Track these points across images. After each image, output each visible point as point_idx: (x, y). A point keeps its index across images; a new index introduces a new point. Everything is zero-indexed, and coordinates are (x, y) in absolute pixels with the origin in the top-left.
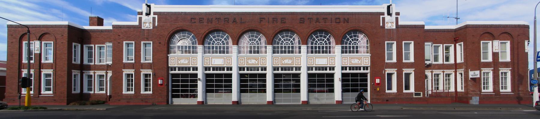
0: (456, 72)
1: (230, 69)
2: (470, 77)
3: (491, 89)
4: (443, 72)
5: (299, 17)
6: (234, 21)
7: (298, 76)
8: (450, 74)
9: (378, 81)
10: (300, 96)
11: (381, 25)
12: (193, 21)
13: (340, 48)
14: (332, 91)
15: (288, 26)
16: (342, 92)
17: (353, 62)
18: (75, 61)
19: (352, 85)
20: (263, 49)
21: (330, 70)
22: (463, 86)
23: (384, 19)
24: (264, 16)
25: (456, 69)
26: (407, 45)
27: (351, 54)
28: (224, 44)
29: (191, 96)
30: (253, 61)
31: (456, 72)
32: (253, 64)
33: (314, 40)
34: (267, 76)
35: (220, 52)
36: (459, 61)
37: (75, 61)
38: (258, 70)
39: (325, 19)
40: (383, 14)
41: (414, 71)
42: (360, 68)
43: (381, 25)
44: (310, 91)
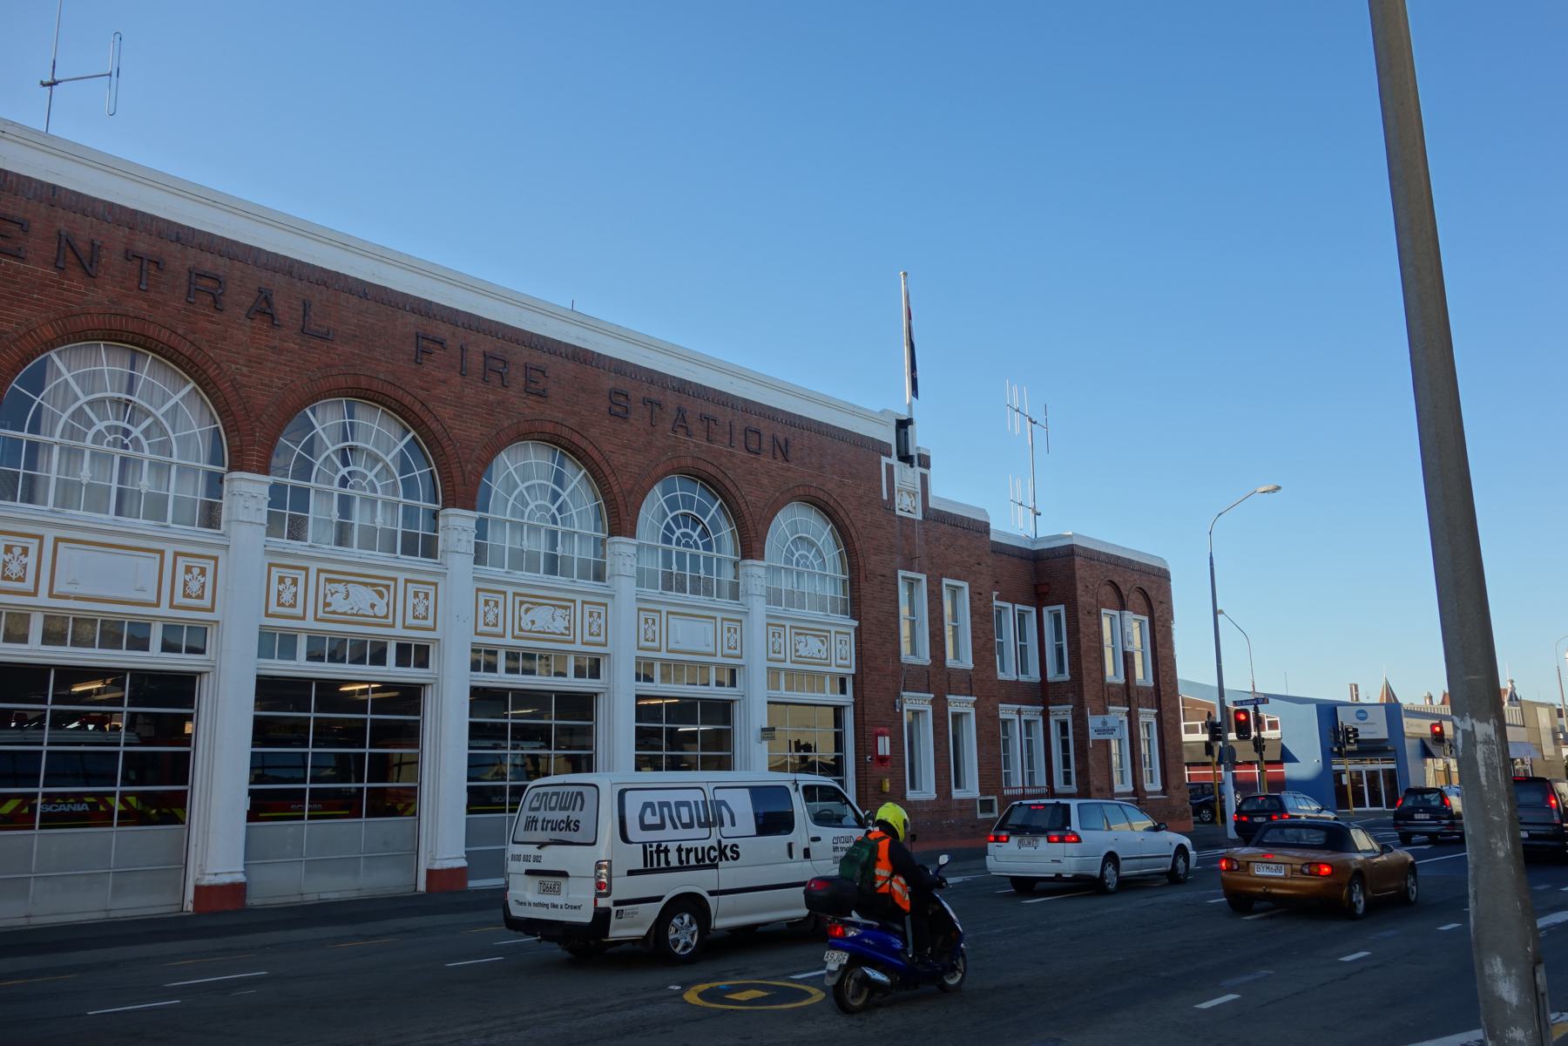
0: (1046, 715)
1: (193, 638)
5: (609, 382)
7: (180, 689)
8: (961, 714)
9: (884, 746)
11: (885, 497)
16: (252, 816)
17: (338, 603)
20: (728, 575)
21: (402, 661)
23: (890, 468)
24: (443, 331)
26: (955, 591)
30: (362, 598)
31: (1046, 715)
32: (356, 617)
39: (425, 345)
41: (975, 705)
43: (885, 497)
44: (266, 805)
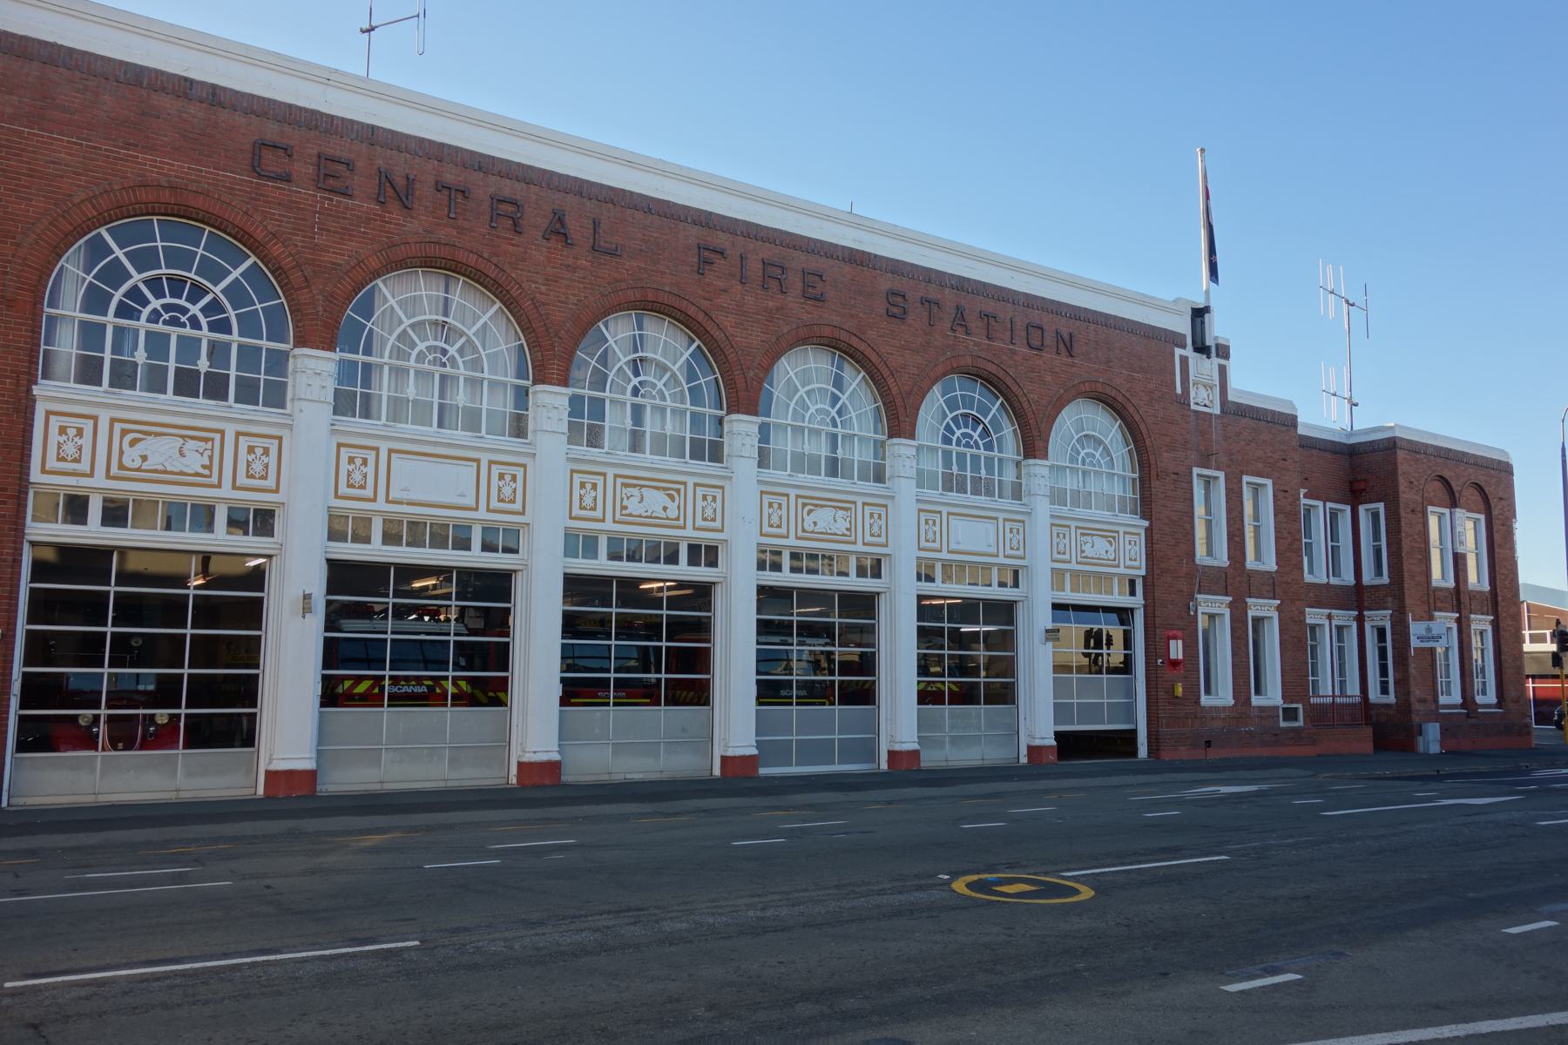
0: (1360, 621)
1: (705, 554)
2: (1415, 643)
3: (1456, 698)
4: (1330, 617)
5: (886, 283)
6: (558, 230)
9: (1176, 650)
10: (873, 726)
11: (1179, 391)
12: (271, 161)
13: (332, 368)
14: (697, 694)
15: (836, 320)
16: (565, 701)
17: (634, 506)
18: (1311, 572)
19: (171, 651)
20: (1009, 475)
22: (1391, 679)
23: (1184, 360)
24: (722, 240)
25: (1361, 609)
26: (1256, 489)
27: (136, 397)
28: (222, 326)
29: (203, 735)
30: (655, 501)
31: (1360, 621)
33: (115, 274)
34: (519, 587)
35: (187, 384)
36: (1368, 577)
37: (1311, 572)
38: (209, 527)
39: (707, 256)
40: (1176, 340)
41: (1278, 608)
42: (204, 517)
43: (1179, 391)
